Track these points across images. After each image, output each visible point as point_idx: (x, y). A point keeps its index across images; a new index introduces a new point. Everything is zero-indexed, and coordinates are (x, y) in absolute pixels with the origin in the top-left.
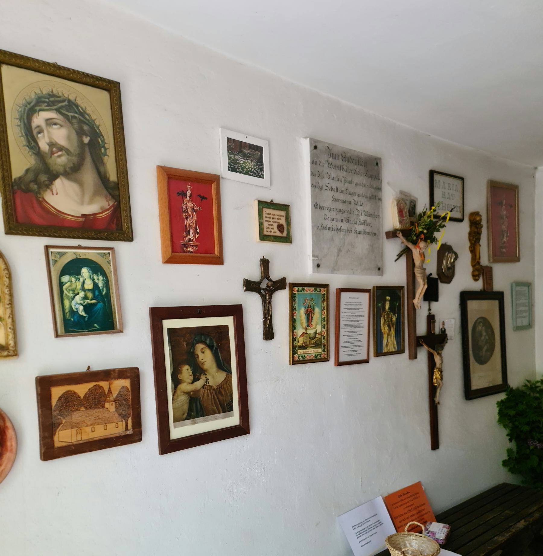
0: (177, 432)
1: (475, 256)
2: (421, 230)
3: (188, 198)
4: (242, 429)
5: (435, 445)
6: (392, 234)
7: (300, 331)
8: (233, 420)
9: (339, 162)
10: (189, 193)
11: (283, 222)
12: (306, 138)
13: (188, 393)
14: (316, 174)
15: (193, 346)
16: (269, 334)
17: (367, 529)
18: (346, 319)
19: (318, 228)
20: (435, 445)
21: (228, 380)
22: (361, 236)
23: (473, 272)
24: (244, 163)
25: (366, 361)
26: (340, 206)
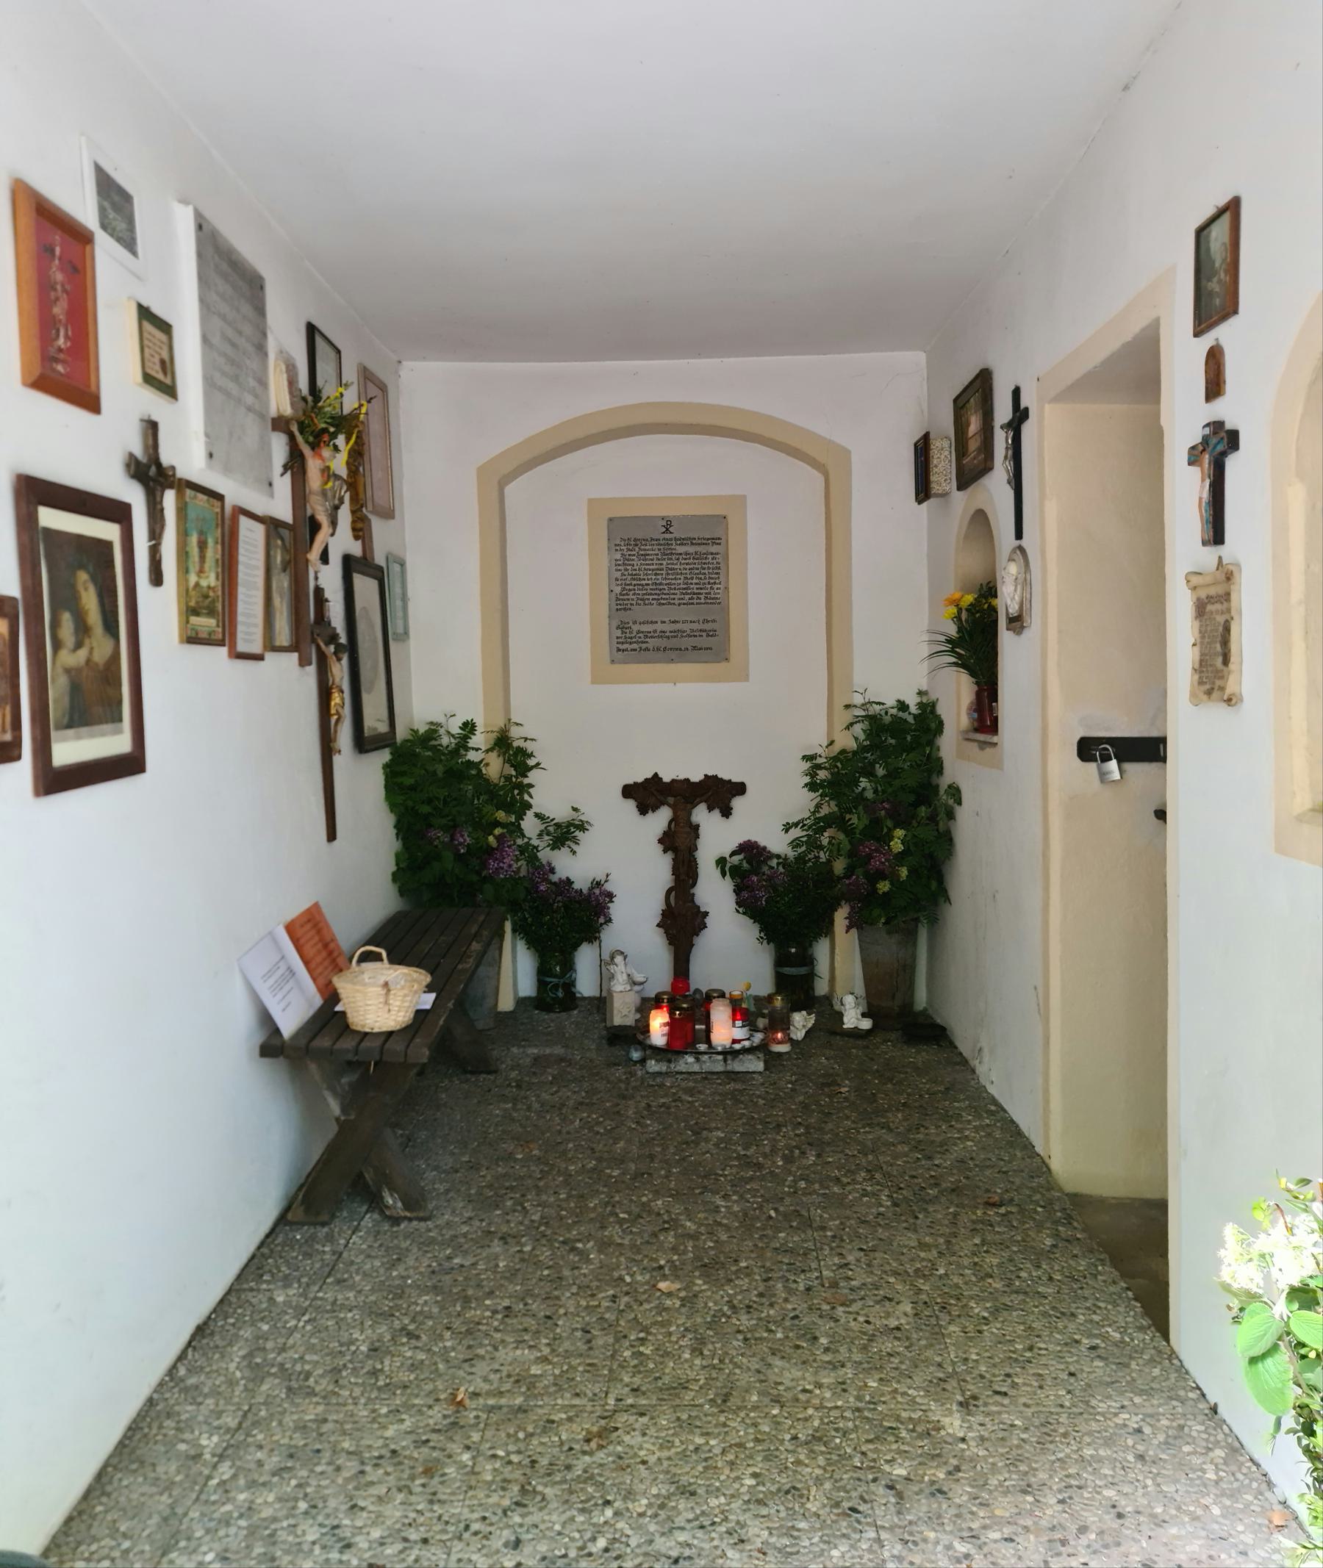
0: (67, 751)
1: (357, 494)
2: (323, 426)
3: (57, 262)
4: (131, 764)
5: (332, 836)
6: (279, 424)
7: (193, 579)
8: (119, 743)
9: (225, 266)
10: (58, 250)
11: (165, 355)
12: (185, 202)
13: (68, 671)
14: (203, 280)
15: (74, 574)
16: (157, 578)
17: (677, 602)
18: (253, 562)
19: (210, 384)
20: (332, 836)
21: (116, 656)
22: (251, 415)
23: (353, 522)
24: (115, 219)
25: (259, 658)
26: (229, 350)
